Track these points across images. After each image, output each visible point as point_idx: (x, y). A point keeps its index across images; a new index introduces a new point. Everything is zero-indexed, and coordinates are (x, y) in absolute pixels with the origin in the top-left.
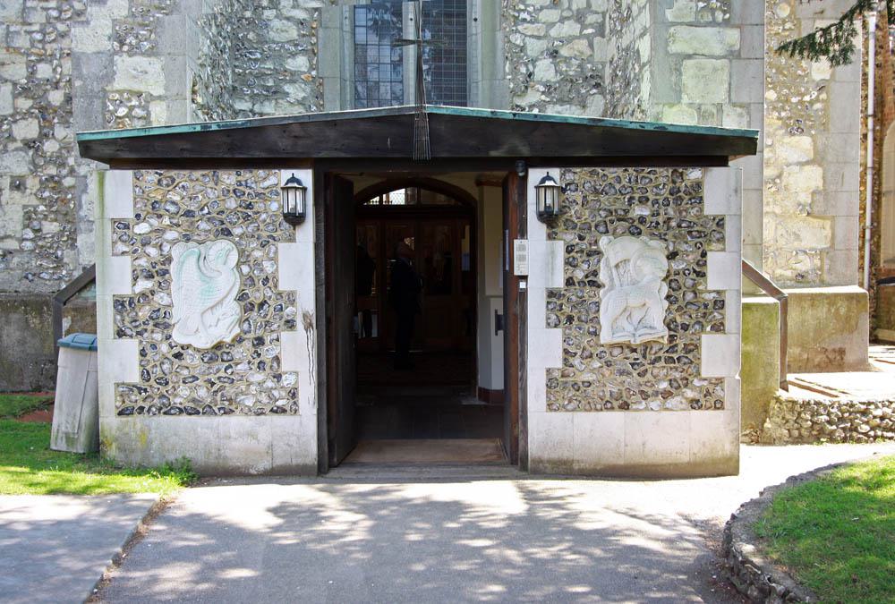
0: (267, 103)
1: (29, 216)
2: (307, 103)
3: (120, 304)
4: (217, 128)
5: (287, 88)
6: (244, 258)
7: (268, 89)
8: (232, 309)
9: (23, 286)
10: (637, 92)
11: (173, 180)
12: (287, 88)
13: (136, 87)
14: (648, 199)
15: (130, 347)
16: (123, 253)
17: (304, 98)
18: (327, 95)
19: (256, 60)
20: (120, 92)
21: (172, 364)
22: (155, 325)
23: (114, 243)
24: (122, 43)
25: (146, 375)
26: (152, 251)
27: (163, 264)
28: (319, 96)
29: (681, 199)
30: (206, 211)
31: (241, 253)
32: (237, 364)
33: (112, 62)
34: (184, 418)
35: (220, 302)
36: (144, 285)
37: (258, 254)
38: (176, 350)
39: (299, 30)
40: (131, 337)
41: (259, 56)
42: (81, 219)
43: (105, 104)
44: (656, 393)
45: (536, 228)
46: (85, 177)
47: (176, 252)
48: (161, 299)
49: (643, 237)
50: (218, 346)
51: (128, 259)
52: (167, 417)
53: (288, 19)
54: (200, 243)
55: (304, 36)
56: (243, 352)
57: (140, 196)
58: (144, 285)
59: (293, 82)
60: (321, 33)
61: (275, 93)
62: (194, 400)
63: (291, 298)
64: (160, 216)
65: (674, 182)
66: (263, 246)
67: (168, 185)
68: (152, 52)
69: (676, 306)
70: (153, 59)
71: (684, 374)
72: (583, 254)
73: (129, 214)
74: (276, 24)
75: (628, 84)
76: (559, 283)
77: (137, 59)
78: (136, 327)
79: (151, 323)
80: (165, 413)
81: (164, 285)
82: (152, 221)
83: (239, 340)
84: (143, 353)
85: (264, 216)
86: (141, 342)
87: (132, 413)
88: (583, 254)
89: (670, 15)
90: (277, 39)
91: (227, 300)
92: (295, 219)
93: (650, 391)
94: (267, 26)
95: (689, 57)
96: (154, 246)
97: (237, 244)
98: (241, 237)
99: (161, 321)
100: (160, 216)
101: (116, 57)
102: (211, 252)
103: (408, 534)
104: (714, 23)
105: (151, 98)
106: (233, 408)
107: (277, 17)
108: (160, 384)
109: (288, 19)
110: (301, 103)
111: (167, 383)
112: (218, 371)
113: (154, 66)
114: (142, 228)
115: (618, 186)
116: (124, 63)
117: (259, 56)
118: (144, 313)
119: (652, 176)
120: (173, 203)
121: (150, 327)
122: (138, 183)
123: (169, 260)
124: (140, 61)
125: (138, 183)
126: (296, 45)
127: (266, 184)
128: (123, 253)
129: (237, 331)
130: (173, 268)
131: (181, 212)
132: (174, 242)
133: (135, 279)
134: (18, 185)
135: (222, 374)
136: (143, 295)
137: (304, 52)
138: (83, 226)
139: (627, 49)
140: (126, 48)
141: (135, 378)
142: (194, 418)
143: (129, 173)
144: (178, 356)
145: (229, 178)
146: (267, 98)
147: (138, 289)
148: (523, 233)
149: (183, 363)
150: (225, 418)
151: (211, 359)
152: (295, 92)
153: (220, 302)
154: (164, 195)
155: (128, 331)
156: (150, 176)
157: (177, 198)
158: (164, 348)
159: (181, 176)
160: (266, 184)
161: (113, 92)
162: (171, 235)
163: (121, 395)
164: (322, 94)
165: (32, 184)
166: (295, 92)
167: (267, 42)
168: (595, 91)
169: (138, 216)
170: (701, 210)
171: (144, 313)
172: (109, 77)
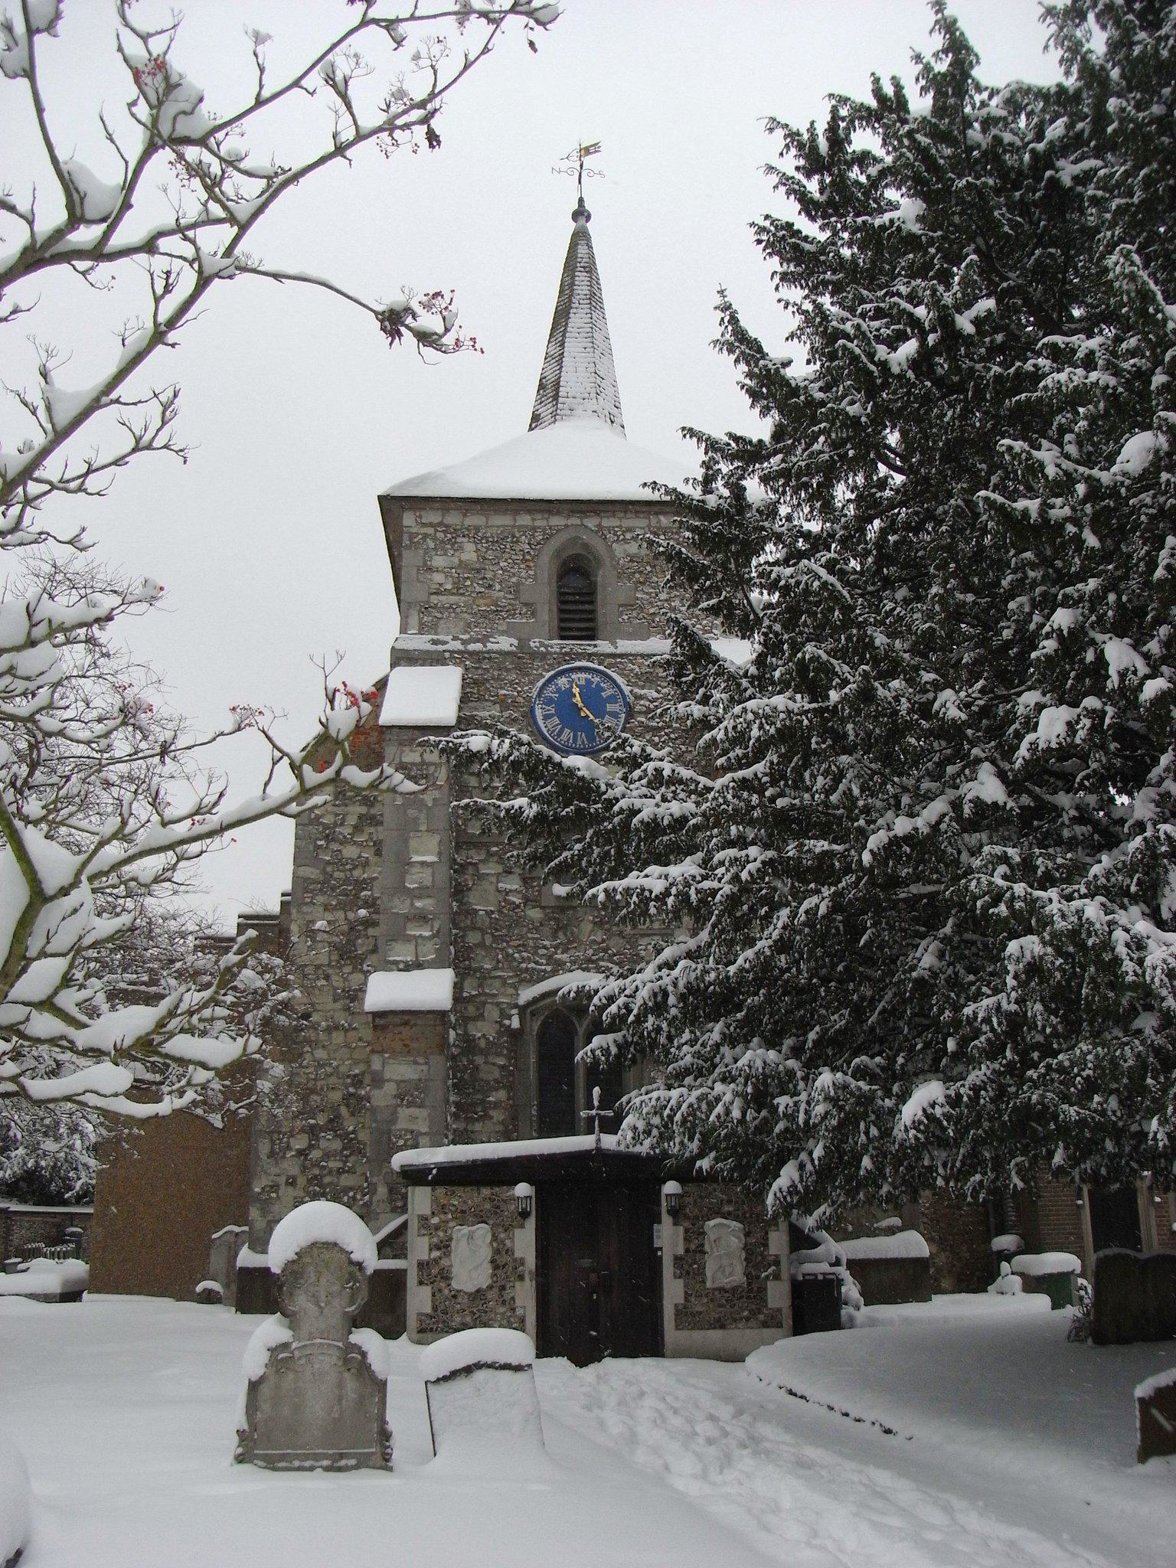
4: (531, 1224)
5: (492, 1113)
6: (495, 1238)
12: (492, 1113)
13: (412, 1127)
15: (426, 1291)
25: (435, 1308)
26: (441, 1234)
31: (494, 1235)
36: (436, 1254)
45: (667, 1219)
48: (444, 1262)
56: (492, 1295)
57: (435, 1200)
58: (436, 1254)
63: (522, 1262)
73: (427, 1212)
76: (681, 1251)
77: (411, 1110)
81: (447, 1254)
83: (490, 1287)
84: (433, 1295)
88: (695, 1239)
92: (524, 1215)
99: (445, 1276)
113: (422, 1113)
114: (435, 1220)
116: (404, 1113)
124: (413, 1111)
130: (453, 1244)
137: (504, 1087)
141: (428, 1310)
143: (429, 1189)
145: (486, 1191)
156: (440, 1191)
158: (446, 1291)
159: (460, 1191)
165: (301, 1181)
171: (434, 1272)
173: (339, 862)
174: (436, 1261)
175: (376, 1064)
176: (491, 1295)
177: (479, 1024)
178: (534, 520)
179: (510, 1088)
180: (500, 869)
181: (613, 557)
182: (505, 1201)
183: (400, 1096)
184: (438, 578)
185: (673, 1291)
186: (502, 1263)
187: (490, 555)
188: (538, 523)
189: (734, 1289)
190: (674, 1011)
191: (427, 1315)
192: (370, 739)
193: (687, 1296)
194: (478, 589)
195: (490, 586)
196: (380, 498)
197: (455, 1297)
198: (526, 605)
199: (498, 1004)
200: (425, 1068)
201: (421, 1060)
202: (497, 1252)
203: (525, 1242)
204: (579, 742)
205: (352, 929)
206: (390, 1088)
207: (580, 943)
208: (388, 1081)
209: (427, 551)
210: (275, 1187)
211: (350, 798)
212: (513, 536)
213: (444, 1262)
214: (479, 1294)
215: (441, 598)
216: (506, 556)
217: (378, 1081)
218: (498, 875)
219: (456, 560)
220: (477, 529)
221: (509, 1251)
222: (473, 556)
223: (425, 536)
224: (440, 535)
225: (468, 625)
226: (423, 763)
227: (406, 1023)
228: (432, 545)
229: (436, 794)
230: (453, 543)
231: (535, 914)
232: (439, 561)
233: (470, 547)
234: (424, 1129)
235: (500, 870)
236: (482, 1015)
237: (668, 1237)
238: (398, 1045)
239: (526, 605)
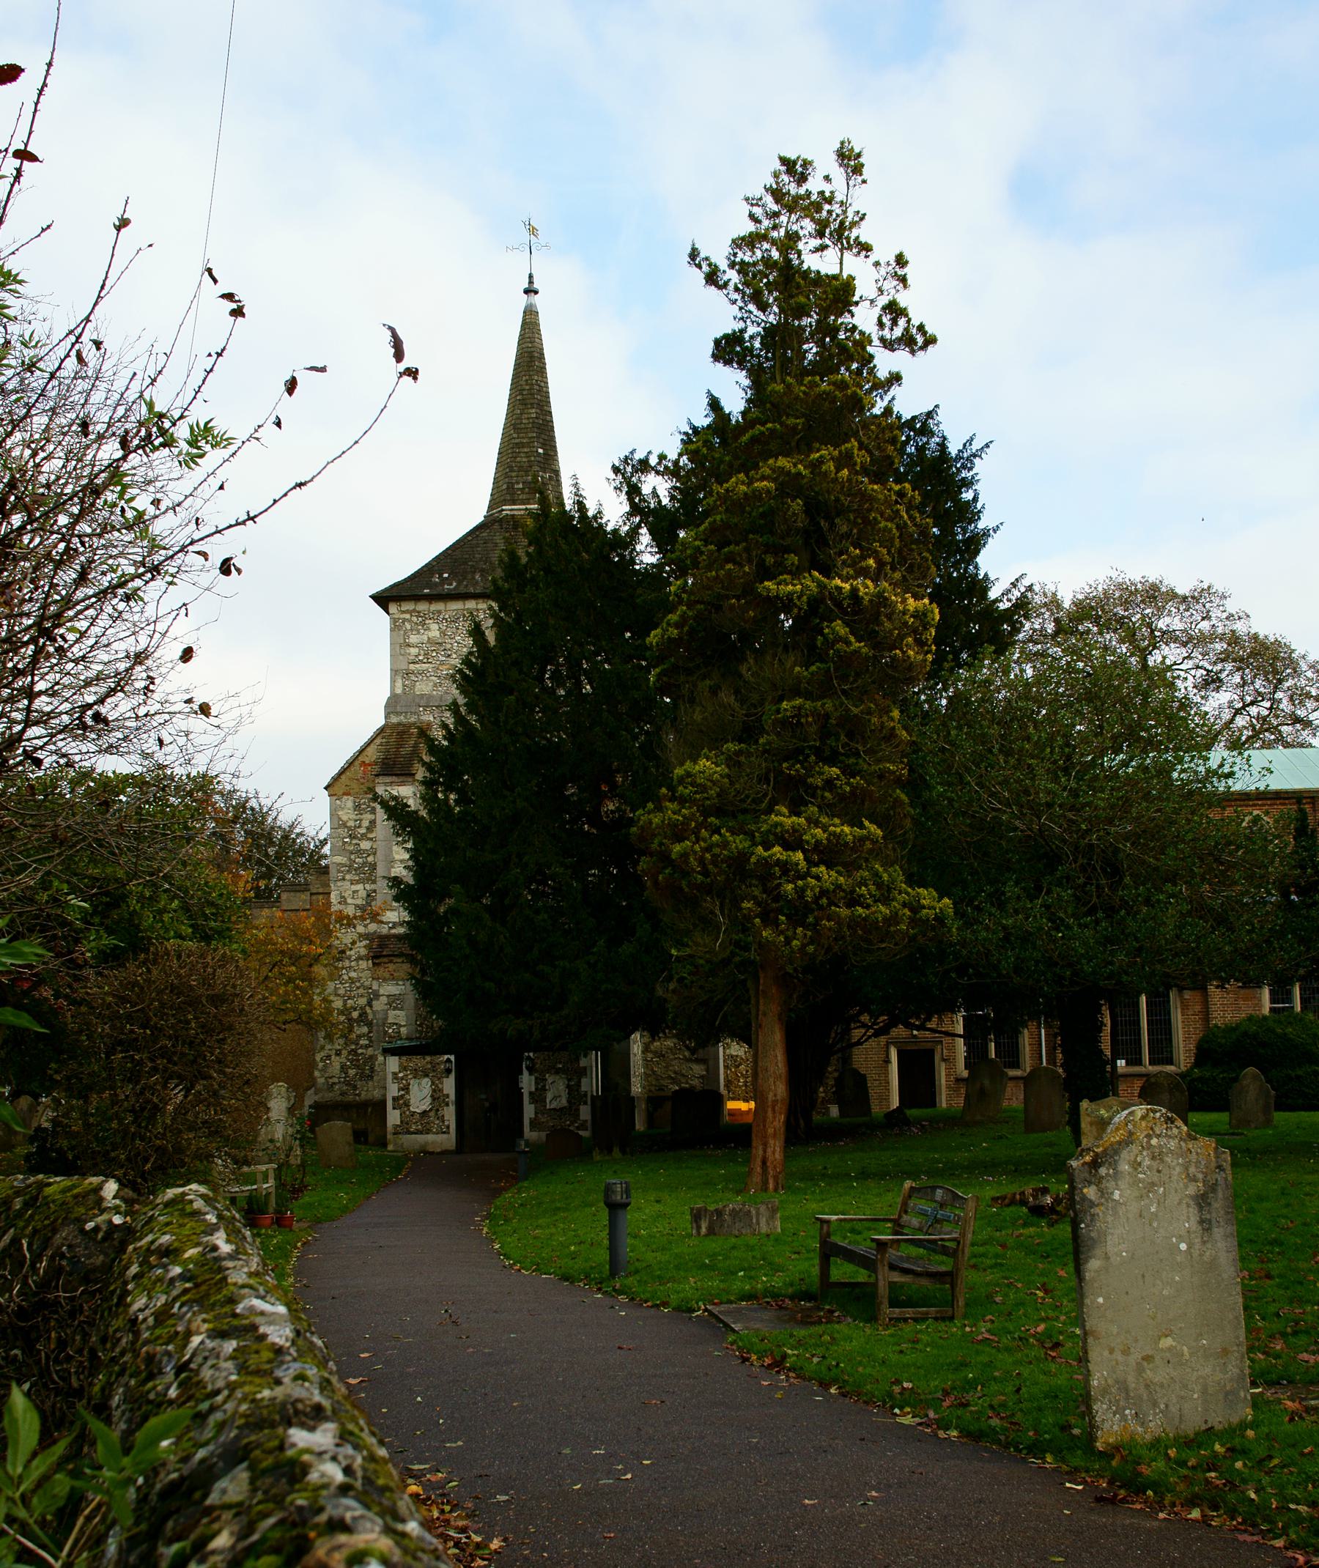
1: (344, 1068)
3: (394, 1099)
4: (452, 1076)
6: (433, 1083)
8: (429, 1100)
9: (339, 1099)
15: (397, 1112)
45: (525, 1072)
50: (425, 1112)
56: (432, 1114)
63: (448, 1096)
68: (401, 1009)
72: (540, 1081)
76: (533, 1089)
81: (408, 1093)
92: (448, 1071)
99: (407, 1104)
103: (401, 924)
116: (392, 1013)
124: (397, 1012)
134: (338, 1053)
145: (428, 1058)
148: (521, 1073)
156: (404, 1058)
165: (345, 1053)
172: (386, 1018)
173: (359, 852)
174: (402, 1096)
176: (432, 1114)
183: (389, 1004)
184: (414, 651)
185: (529, 1111)
186: (437, 1097)
188: (480, 606)
189: (561, 1109)
190: (1130, 770)
193: (536, 1113)
202: (434, 1091)
203: (449, 1085)
205: (368, 895)
206: (384, 1000)
210: (329, 1057)
214: (424, 1113)
219: (425, 638)
220: (439, 612)
221: (441, 1090)
222: (437, 634)
223: (404, 620)
224: (414, 619)
225: (435, 685)
227: (391, 962)
228: (408, 627)
232: (414, 639)
233: (434, 627)
237: (527, 1082)
238: (387, 975)
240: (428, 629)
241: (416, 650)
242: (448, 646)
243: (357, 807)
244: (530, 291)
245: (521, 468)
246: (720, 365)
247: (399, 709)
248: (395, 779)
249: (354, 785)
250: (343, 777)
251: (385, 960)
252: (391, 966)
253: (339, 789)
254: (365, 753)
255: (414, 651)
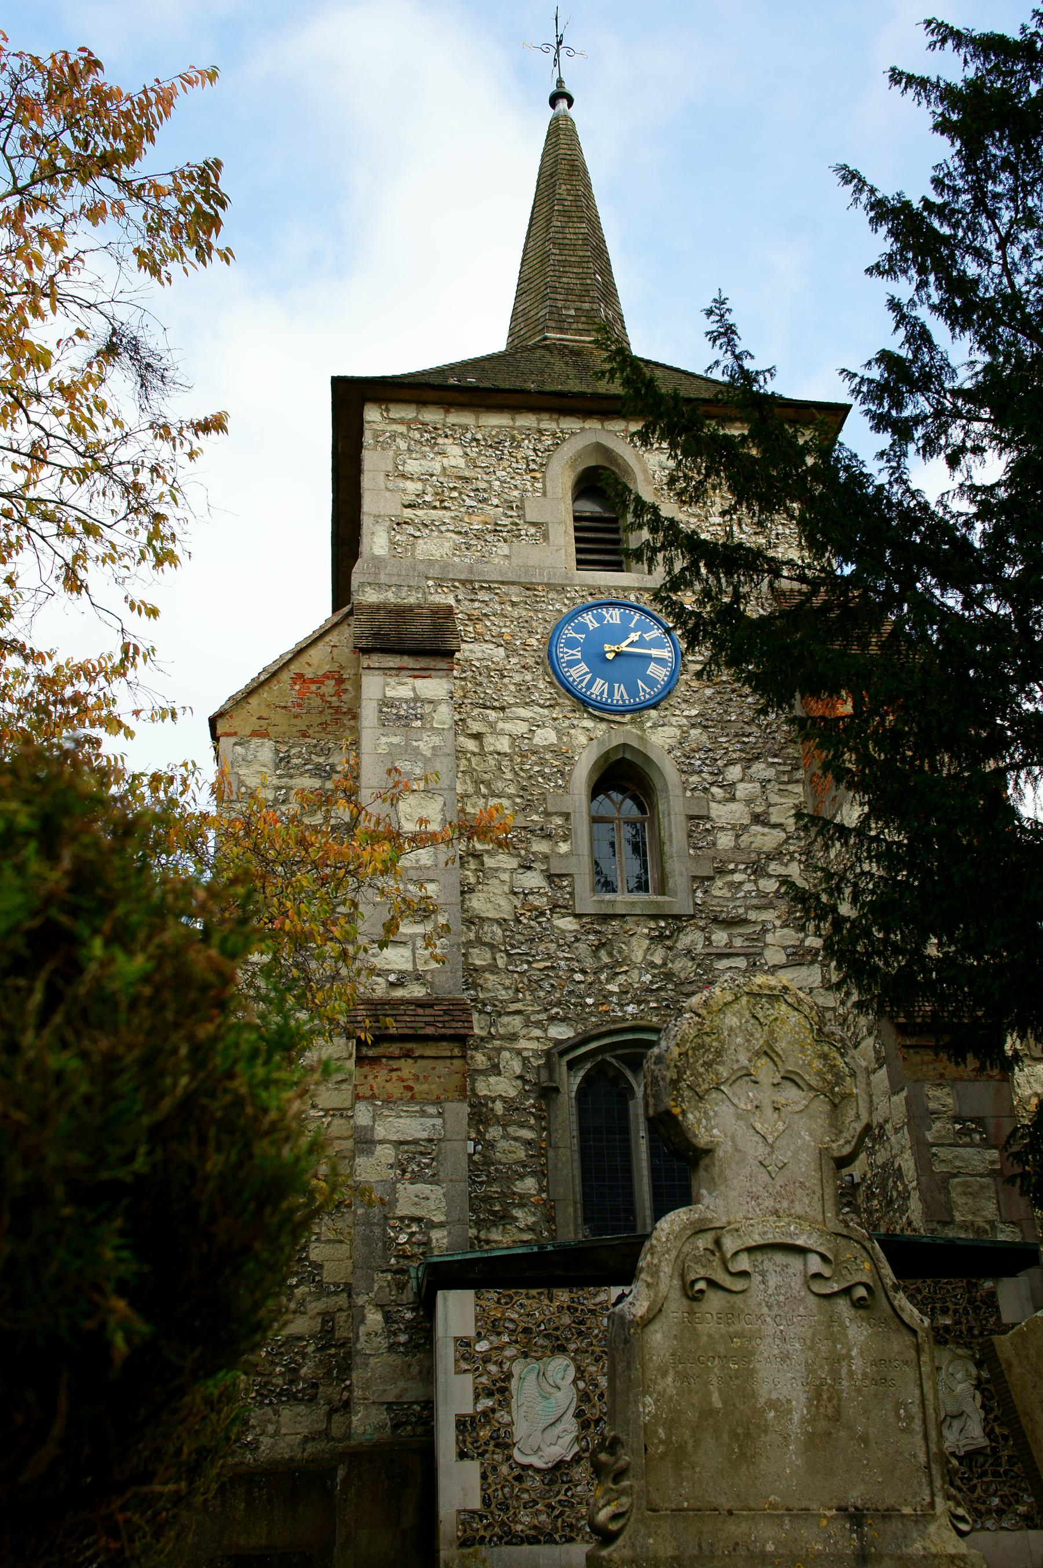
0: (494, 1229)
2: (538, 1229)
3: (462, 1424)
5: (517, 1213)
7: (495, 1213)
8: (570, 1425)
10: (903, 1210)
11: (511, 1298)
12: (517, 1213)
13: (418, 1213)
14: (948, 1309)
15: (473, 1468)
16: (466, 1371)
17: (534, 1223)
18: (560, 1219)
19: (482, 1183)
20: (401, 1219)
21: (512, 1487)
22: (496, 1445)
23: (456, 1361)
24: (404, 1171)
25: (486, 1501)
26: (493, 1368)
27: (503, 1381)
28: (550, 1219)
29: (979, 1308)
30: (543, 1327)
31: (578, 1369)
32: (576, 1486)
33: (394, 1190)
34: (526, 1548)
35: (559, 1419)
36: (486, 1403)
37: (593, 1369)
38: (516, 1472)
39: (526, 1150)
40: (472, 1458)
41: (484, 1178)
42: (358, 1352)
43: (385, 1230)
44: (989, 1511)
46: (363, 1307)
47: (517, 1368)
49: (950, 1346)
50: (559, 1465)
51: (470, 1377)
52: (509, 1547)
53: (516, 1139)
54: (538, 1359)
55: (532, 1156)
58: (486, 1403)
59: (521, 1206)
60: (551, 1154)
61: (502, 1218)
62: (535, 1527)
64: (499, 1334)
65: (970, 1292)
66: (597, 1360)
67: (506, 1303)
69: (992, 1416)
70: (434, 1187)
71: (1013, 1490)
74: (503, 1144)
75: (890, 1202)
77: (419, 1186)
78: (478, 1448)
79: (492, 1443)
80: (507, 1543)
81: (505, 1403)
82: (492, 1338)
83: (577, 1459)
84: (484, 1476)
85: (596, 1331)
86: (482, 1464)
87: (473, 1544)
89: (929, 1137)
90: (504, 1161)
91: (566, 1417)
93: (983, 1508)
94: (493, 1146)
95: (955, 1176)
96: (495, 1363)
97: (573, 1359)
98: (576, 1351)
99: (503, 1443)
100: (499, 1334)
101: (398, 1185)
102: (550, 1368)
104: (971, 1145)
105: (433, 1225)
106: (573, 1535)
107: (503, 1137)
108: (501, 1510)
109: (516, 1139)
110: (529, 1229)
111: (508, 1509)
112: (558, 1493)
113: (434, 1192)
114: (482, 1346)
115: (919, 1297)
117: (484, 1178)
118: (484, 1433)
119: (949, 1287)
120: (512, 1320)
121: (491, 1448)
122: (480, 1302)
123: (509, 1376)
124: (422, 1188)
125: (480, 1302)
126: (524, 1166)
127: (598, 1299)
128: (466, 1371)
129: (576, 1448)
130: (514, 1384)
131: (520, 1329)
132: (513, 1359)
133: (477, 1398)
135: (561, 1497)
136: (484, 1413)
137: (533, 1174)
138: (358, 1360)
139: (884, 1166)
140: (408, 1175)
142: (535, 1548)
143: (470, 1293)
144: (519, 1478)
145: (563, 1296)
146: (495, 1224)
147: (480, 1408)
149: (524, 1486)
150: (566, 1545)
151: (551, 1480)
152: (524, 1217)
153: (559, 1419)
154: (503, 1314)
155: (470, 1453)
156: (492, 1295)
157: (515, 1316)
158: (504, 1469)
160: (598, 1299)
161: (394, 1218)
162: (509, 1352)
163: (463, 1524)
164: (554, 1218)
166: (524, 1217)
167: (493, 1164)
168: (847, 1209)
169: (479, 1334)
170: (999, 1318)
171: (484, 1433)
174: (487, 1415)
175: (363, 1115)
177: (492, 1079)
178: (539, 421)
179: (540, 1174)
180: (514, 863)
181: (645, 471)
182: (592, 1312)
184: (413, 487)
187: (482, 462)
188: (544, 425)
191: (473, 1512)
192: (323, 689)
194: (469, 502)
195: (484, 500)
196: (333, 378)
197: (519, 1478)
198: (534, 524)
199: (519, 1052)
200: (439, 1121)
201: (431, 1110)
202: (584, 1397)
204: (617, 697)
206: (385, 1153)
207: (633, 965)
208: (381, 1142)
209: (398, 453)
211: (297, 767)
212: (513, 439)
213: (502, 1416)
215: (419, 512)
216: (506, 464)
217: (365, 1142)
218: (513, 871)
219: (437, 468)
222: (461, 462)
223: (393, 436)
224: (416, 435)
226: (416, 699)
227: (407, 1055)
228: (403, 446)
229: (436, 740)
230: (433, 443)
231: (567, 924)
232: (413, 466)
234: (438, 1218)
235: (515, 865)
236: (496, 1066)
238: (395, 1089)
239: (534, 524)
240: (443, 453)
241: (419, 486)
242: (482, 485)
243: (282, 761)
244: (559, 96)
245: (569, 291)
246: (937, 135)
247: (383, 579)
248: (407, 661)
249: (279, 717)
250: (254, 701)
251: (394, 1049)
252: (408, 1068)
253: (242, 722)
254: (304, 658)
255: (413, 487)
